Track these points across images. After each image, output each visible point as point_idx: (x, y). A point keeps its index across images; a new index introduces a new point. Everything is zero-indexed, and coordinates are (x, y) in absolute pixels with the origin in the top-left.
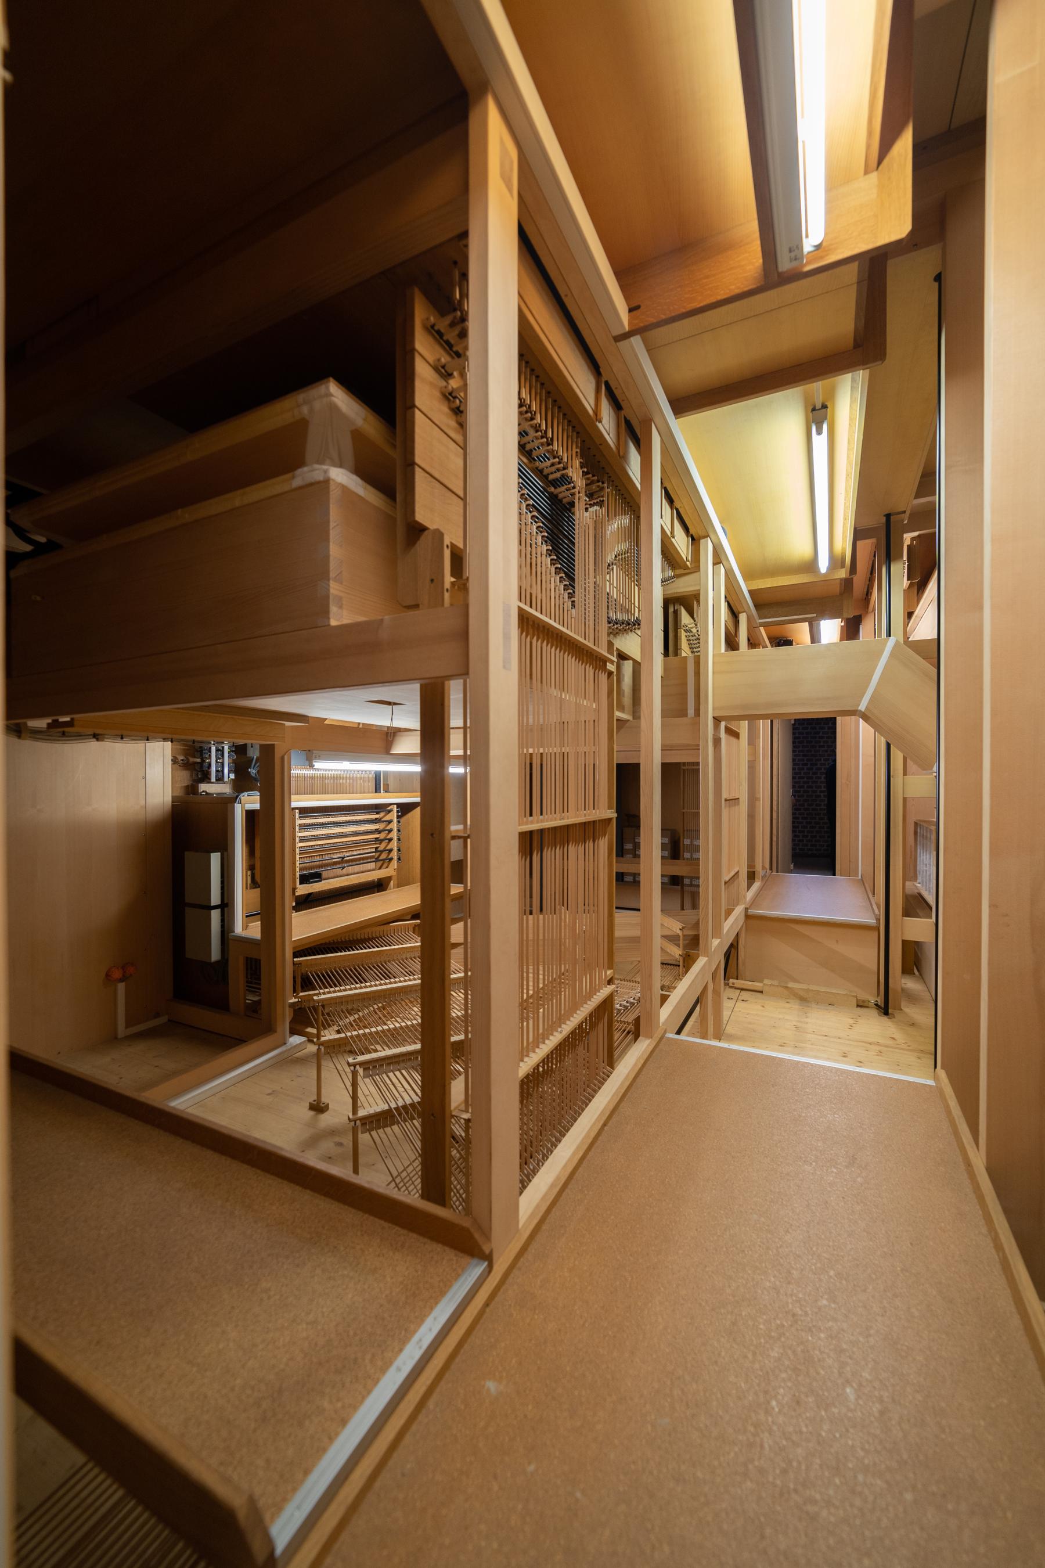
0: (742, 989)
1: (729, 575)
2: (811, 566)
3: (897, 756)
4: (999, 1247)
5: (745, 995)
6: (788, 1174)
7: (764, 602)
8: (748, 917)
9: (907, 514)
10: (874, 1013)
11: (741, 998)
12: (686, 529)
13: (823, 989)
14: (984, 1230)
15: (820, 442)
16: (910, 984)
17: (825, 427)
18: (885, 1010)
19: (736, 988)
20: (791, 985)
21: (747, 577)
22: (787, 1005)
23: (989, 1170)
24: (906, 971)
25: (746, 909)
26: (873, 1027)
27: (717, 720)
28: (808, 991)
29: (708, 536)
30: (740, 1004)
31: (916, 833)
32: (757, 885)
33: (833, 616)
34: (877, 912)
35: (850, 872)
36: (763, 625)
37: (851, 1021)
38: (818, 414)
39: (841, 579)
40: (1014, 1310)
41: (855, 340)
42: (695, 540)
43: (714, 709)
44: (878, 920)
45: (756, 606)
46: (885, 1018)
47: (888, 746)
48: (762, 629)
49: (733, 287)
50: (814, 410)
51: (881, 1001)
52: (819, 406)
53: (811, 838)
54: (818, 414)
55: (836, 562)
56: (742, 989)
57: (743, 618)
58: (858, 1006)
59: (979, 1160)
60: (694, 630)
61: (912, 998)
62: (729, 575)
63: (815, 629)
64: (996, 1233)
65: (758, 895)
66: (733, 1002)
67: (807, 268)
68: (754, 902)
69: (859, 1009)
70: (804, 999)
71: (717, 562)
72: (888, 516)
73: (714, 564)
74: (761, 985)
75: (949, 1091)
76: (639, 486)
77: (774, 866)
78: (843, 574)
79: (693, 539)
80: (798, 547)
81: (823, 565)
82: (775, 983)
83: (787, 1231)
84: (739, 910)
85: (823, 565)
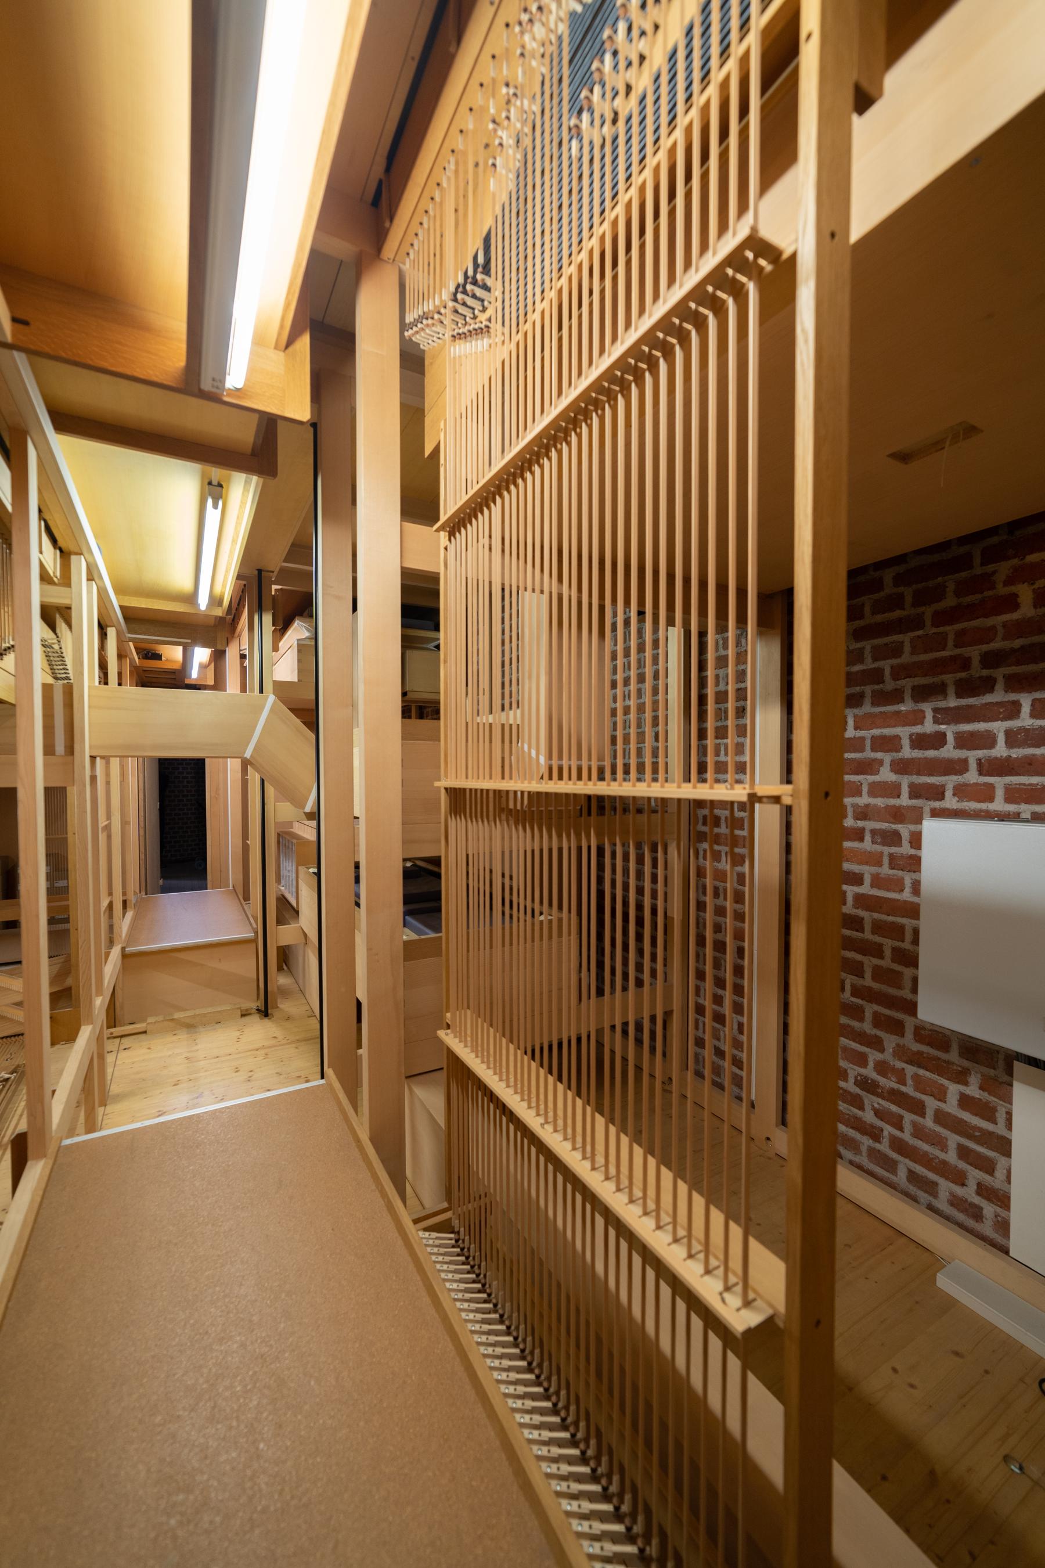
0: (122, 1037)
1: (102, 594)
2: (192, 598)
3: (270, 791)
4: (384, 1194)
5: (126, 1042)
6: (230, 1230)
7: (133, 618)
8: (125, 956)
9: (275, 573)
10: (256, 1018)
11: (122, 1047)
12: (54, 541)
13: (209, 1010)
14: (374, 1187)
15: (213, 515)
16: (283, 980)
17: (220, 503)
18: (265, 1012)
19: (115, 1037)
20: (177, 1015)
21: (119, 590)
22: (175, 1038)
23: (371, 1139)
24: (280, 969)
25: (123, 949)
26: (258, 1032)
27: (93, 758)
28: (194, 1017)
29: (81, 554)
30: (123, 1055)
31: (279, 842)
32: (130, 914)
33: (205, 645)
34: (254, 926)
35: (221, 884)
36: (131, 640)
37: (238, 1033)
38: (214, 490)
39: (216, 617)
40: (397, 1234)
41: (253, 450)
42: (65, 555)
43: (90, 747)
44: (256, 933)
45: (125, 618)
46: (266, 1020)
47: (263, 781)
48: (131, 644)
49: (151, 372)
50: (210, 483)
51: (260, 1004)
52: (215, 482)
53: (179, 848)
54: (214, 490)
55: (215, 601)
56: (122, 1037)
57: (111, 633)
58: (243, 1015)
59: (364, 1136)
60: (56, 647)
61: (284, 993)
62: (102, 594)
63: (189, 653)
64: (382, 1186)
65: (133, 927)
66: (114, 1054)
67: (226, 399)
68: (131, 938)
69: (244, 1019)
70: (190, 1026)
71: (90, 579)
72: (260, 571)
73: (88, 580)
74: (144, 1025)
75: (337, 1085)
76: (10, 508)
77: (147, 888)
78: (219, 612)
79: (61, 551)
80: (180, 579)
81: (203, 602)
82: (160, 1018)
83: (241, 1285)
84: (116, 952)
85: (203, 602)
